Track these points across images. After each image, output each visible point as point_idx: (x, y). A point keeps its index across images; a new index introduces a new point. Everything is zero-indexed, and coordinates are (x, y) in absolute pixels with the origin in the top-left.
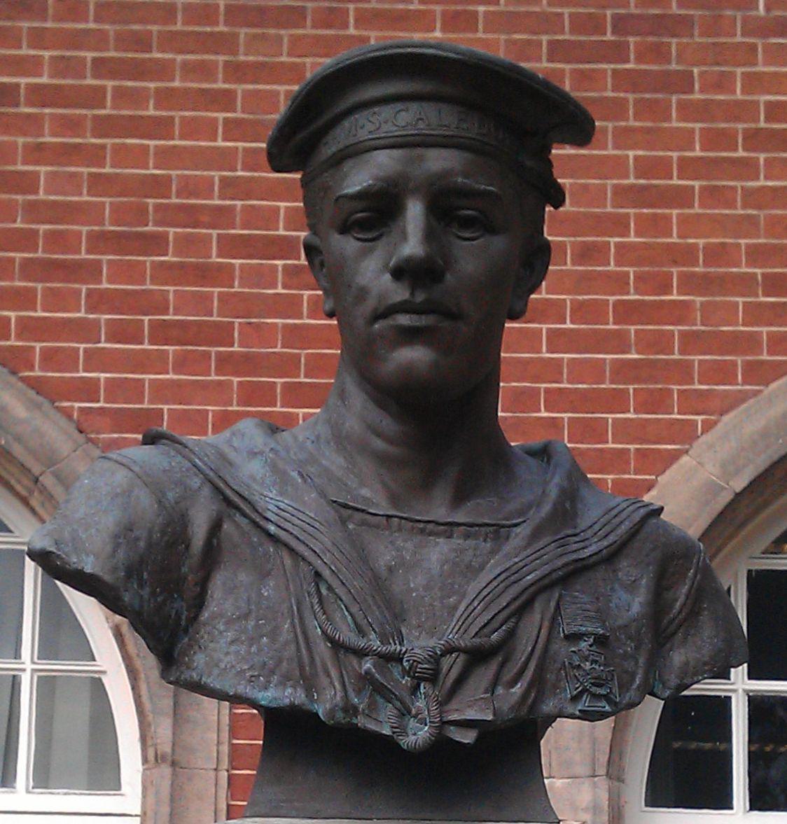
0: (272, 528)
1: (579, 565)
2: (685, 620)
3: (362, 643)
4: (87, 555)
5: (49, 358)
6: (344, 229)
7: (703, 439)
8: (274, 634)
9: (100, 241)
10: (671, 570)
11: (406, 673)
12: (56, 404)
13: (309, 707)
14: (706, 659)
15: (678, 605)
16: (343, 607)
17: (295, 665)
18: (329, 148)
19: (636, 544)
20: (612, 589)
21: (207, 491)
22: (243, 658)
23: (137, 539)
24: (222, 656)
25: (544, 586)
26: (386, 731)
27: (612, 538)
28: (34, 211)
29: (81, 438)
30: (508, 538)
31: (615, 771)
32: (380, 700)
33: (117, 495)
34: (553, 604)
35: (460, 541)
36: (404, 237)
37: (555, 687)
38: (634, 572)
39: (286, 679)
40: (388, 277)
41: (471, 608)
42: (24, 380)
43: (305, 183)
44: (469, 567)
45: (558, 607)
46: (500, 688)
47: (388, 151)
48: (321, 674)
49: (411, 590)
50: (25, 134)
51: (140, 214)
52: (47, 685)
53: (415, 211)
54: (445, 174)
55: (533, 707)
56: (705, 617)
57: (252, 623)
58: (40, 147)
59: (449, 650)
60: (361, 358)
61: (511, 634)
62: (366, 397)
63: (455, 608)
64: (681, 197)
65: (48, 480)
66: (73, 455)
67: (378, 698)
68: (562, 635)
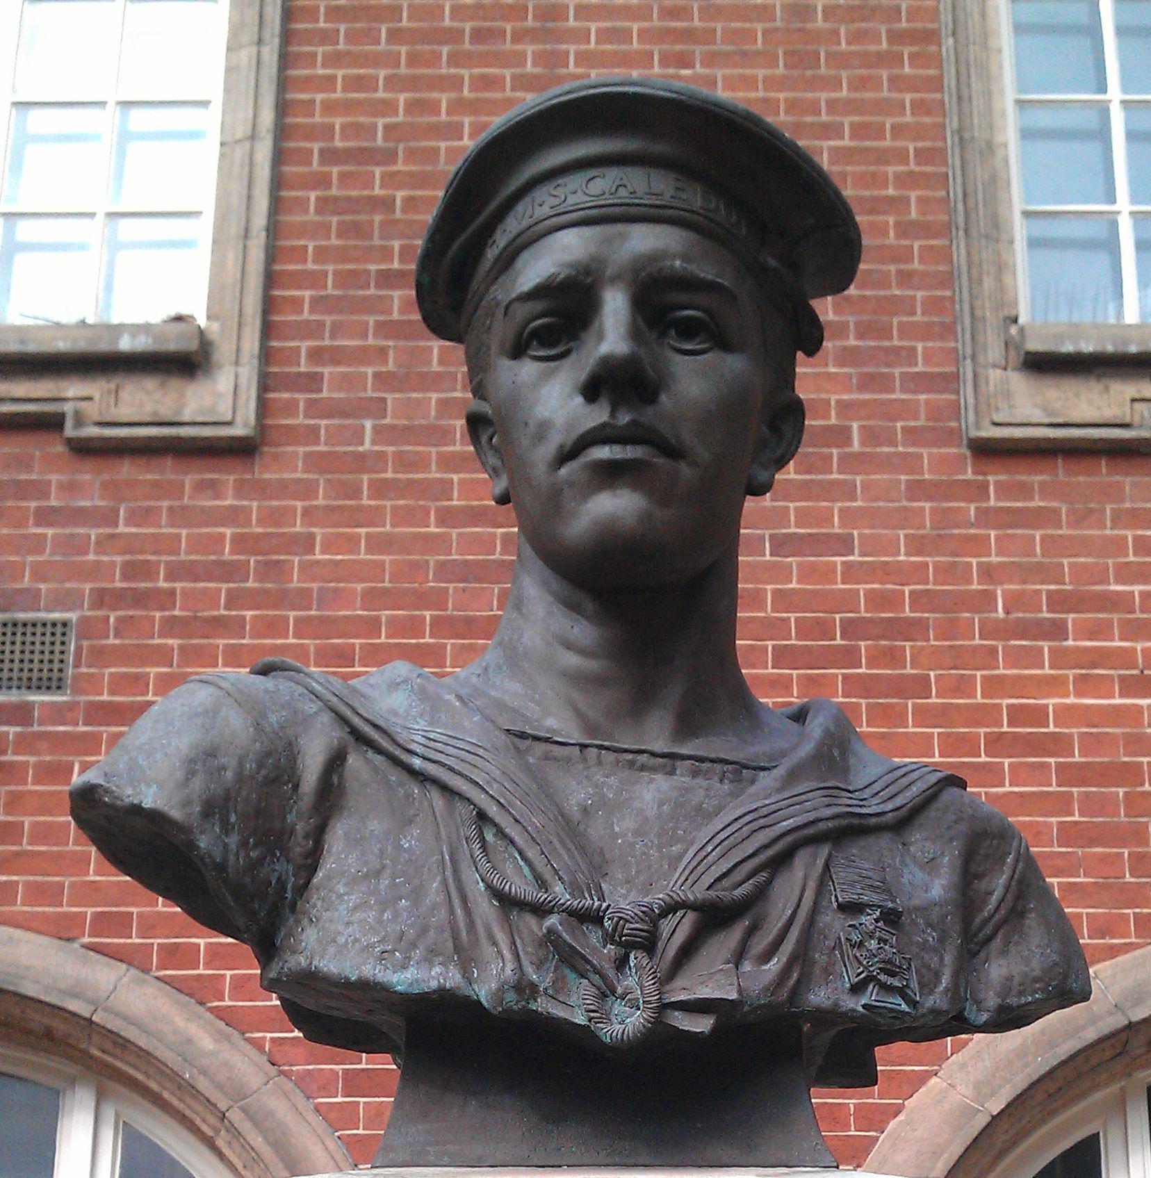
0: (417, 762)
1: (855, 821)
2: (1004, 922)
4: (148, 785)
6: (518, 351)
10: (982, 852)
11: (609, 938)
12: (248, 1035)
13: (468, 992)
14: (1037, 973)
15: (994, 899)
16: (517, 855)
17: (447, 934)
19: (932, 812)
20: (902, 862)
21: (326, 717)
22: (371, 928)
23: (224, 768)
24: (341, 928)
26: (580, 1019)
27: (898, 801)
29: (273, 1070)
30: (753, 782)
32: (571, 976)
33: (196, 715)
34: (820, 862)
35: (687, 779)
37: (827, 972)
38: (931, 848)
39: (432, 955)
40: (579, 400)
41: (703, 853)
44: (699, 809)
45: (827, 866)
46: (746, 963)
47: (575, 230)
48: (484, 941)
49: (615, 836)
53: (615, 307)
54: (654, 257)
55: (795, 992)
56: (1032, 920)
57: (385, 882)
59: (671, 908)
61: (761, 893)
62: (551, 599)
63: (680, 857)
65: (235, 1116)
66: (264, 1089)
67: (567, 971)
68: (835, 905)
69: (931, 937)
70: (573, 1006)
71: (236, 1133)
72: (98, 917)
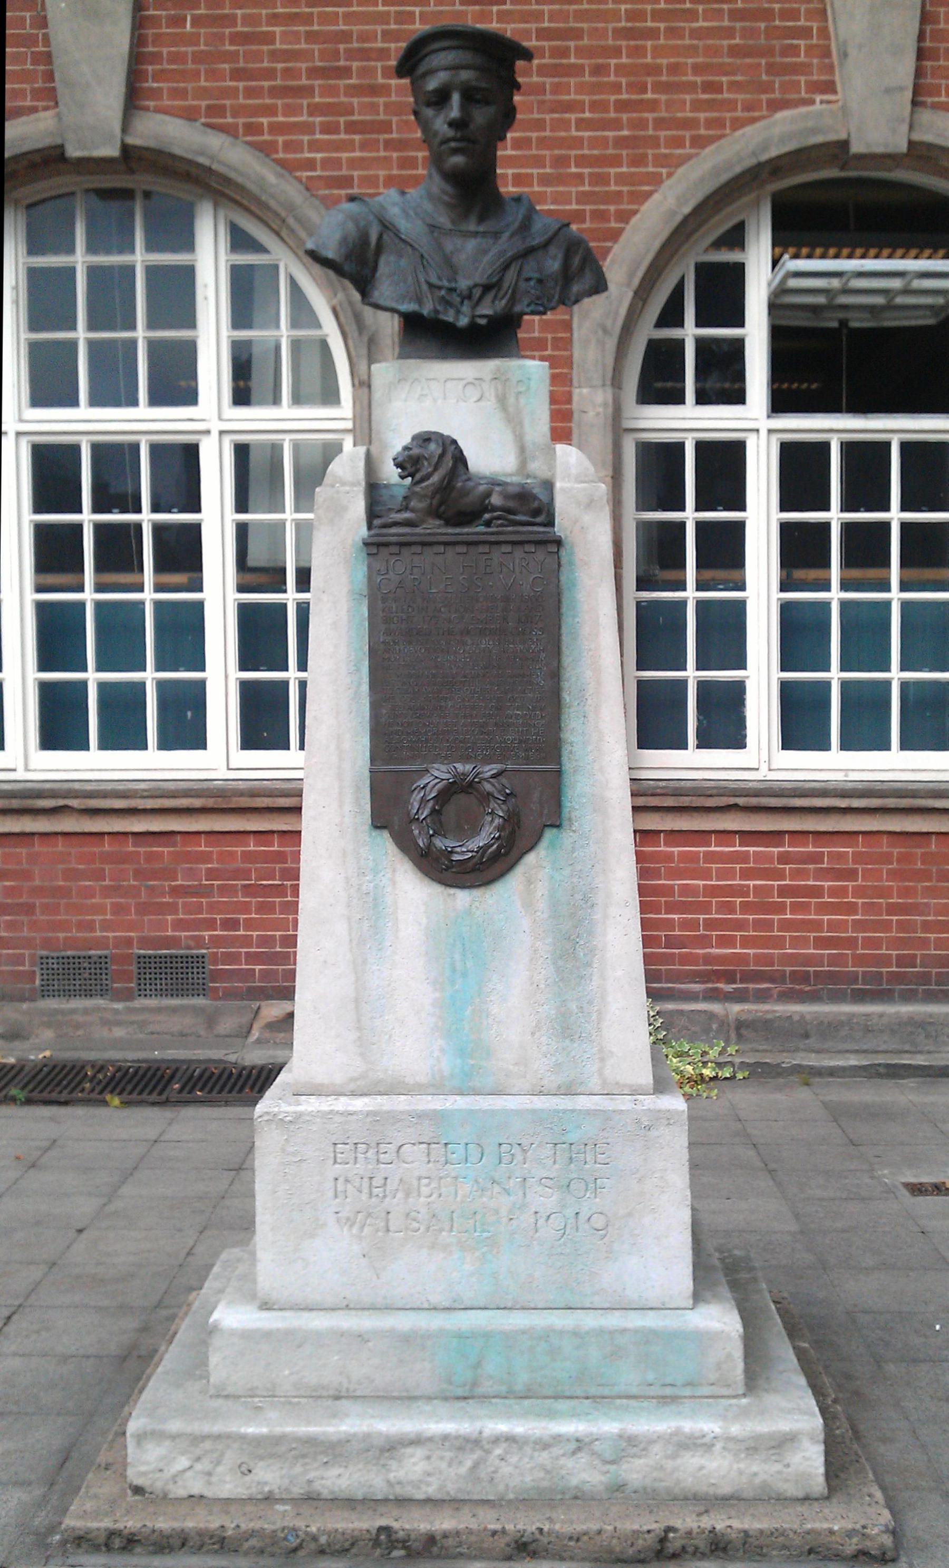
3: (440, 283)
5: (288, 146)
7: (668, 183)
8: (405, 282)
9: (313, 72)
18: (421, 69)
25: (514, 258)
26: (451, 319)
28: (275, 55)
29: (308, 194)
31: (616, 382)
36: (452, 108)
42: (275, 160)
43: (412, 83)
50: (266, 8)
51: (336, 55)
52: (296, 345)
53: (456, 98)
56: (587, 270)
58: (275, 15)
59: (475, 286)
60: (437, 160)
61: (500, 280)
64: (652, 34)
65: (291, 221)
69: (553, 283)
70: (449, 317)
71: (292, 231)
72: (209, 107)
